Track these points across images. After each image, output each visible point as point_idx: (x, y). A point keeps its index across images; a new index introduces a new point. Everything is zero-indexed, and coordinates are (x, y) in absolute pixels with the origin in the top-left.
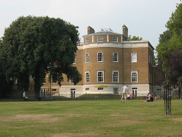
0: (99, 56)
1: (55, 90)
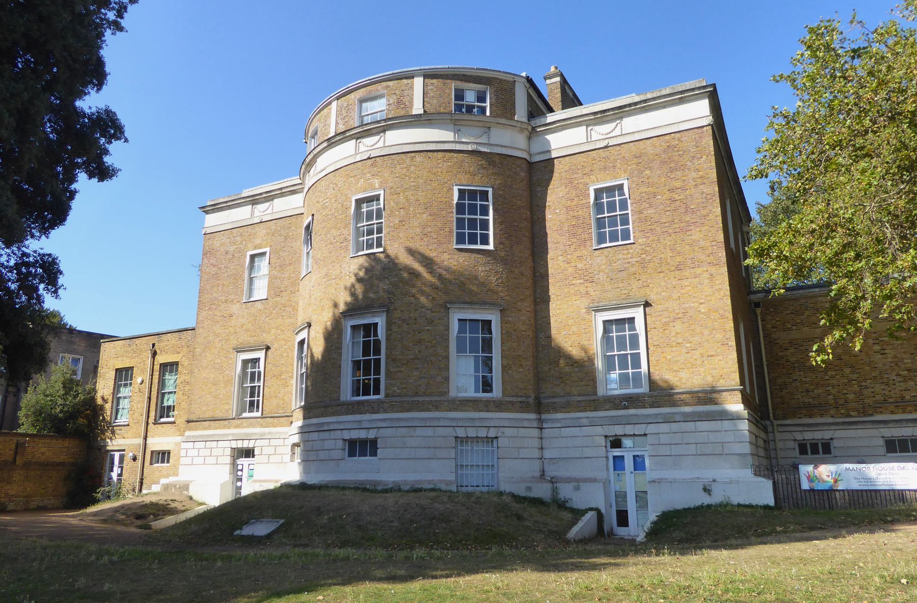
0: (625, 220)
1: (163, 456)
